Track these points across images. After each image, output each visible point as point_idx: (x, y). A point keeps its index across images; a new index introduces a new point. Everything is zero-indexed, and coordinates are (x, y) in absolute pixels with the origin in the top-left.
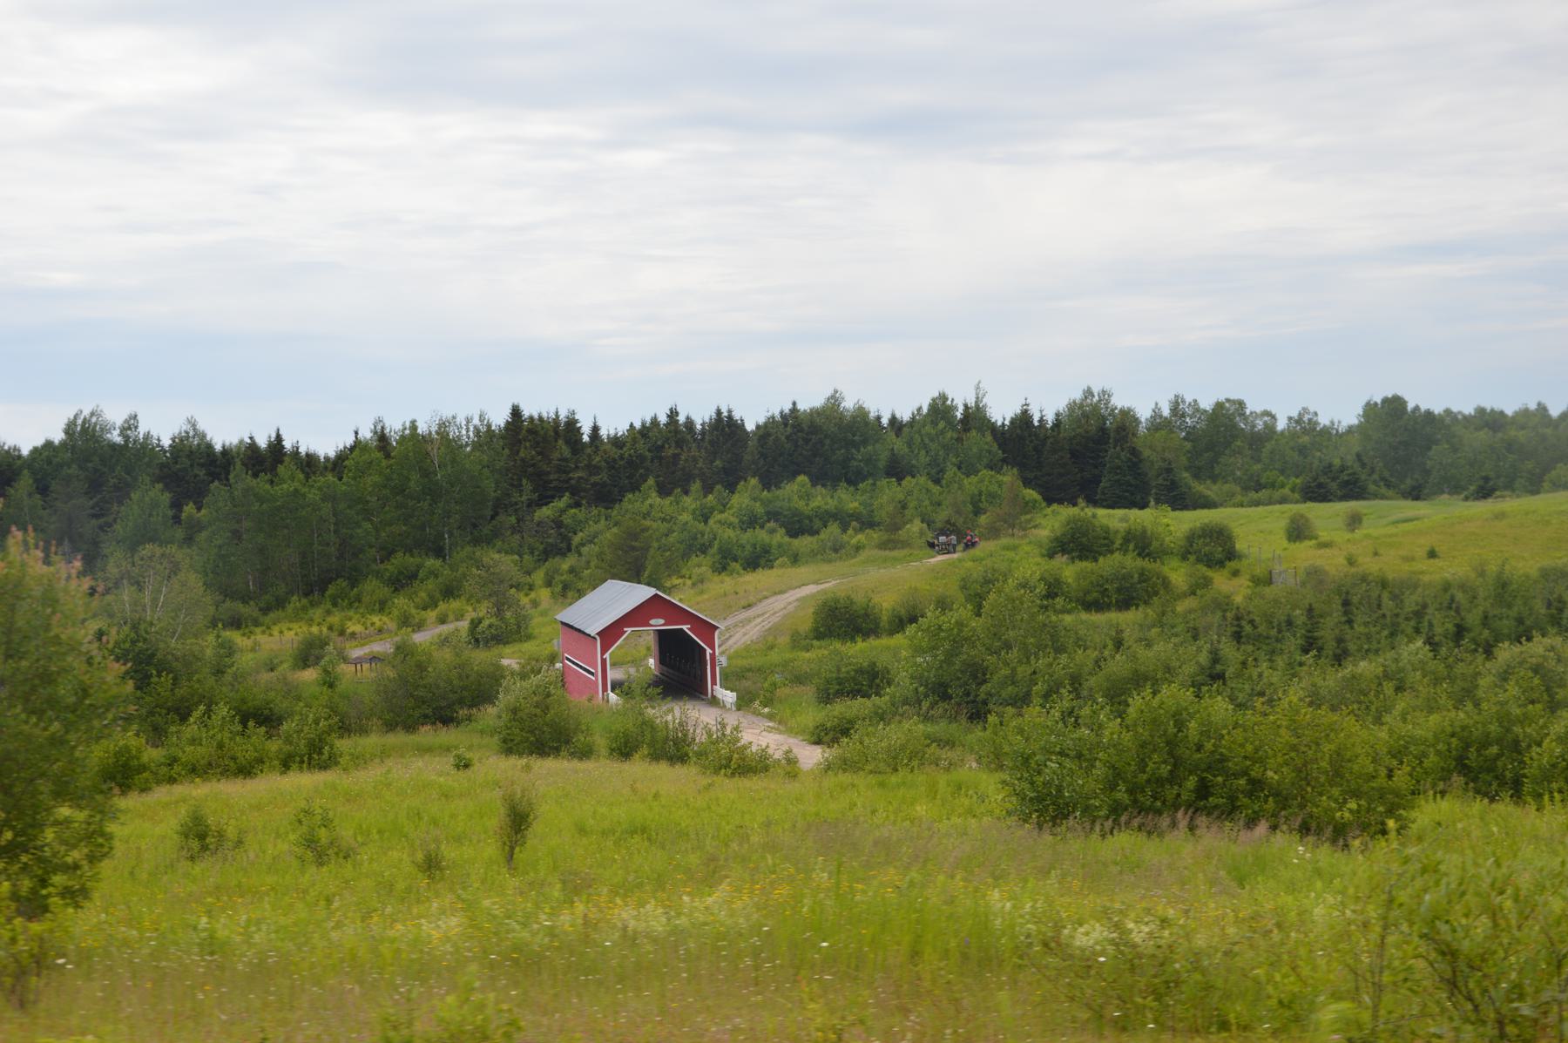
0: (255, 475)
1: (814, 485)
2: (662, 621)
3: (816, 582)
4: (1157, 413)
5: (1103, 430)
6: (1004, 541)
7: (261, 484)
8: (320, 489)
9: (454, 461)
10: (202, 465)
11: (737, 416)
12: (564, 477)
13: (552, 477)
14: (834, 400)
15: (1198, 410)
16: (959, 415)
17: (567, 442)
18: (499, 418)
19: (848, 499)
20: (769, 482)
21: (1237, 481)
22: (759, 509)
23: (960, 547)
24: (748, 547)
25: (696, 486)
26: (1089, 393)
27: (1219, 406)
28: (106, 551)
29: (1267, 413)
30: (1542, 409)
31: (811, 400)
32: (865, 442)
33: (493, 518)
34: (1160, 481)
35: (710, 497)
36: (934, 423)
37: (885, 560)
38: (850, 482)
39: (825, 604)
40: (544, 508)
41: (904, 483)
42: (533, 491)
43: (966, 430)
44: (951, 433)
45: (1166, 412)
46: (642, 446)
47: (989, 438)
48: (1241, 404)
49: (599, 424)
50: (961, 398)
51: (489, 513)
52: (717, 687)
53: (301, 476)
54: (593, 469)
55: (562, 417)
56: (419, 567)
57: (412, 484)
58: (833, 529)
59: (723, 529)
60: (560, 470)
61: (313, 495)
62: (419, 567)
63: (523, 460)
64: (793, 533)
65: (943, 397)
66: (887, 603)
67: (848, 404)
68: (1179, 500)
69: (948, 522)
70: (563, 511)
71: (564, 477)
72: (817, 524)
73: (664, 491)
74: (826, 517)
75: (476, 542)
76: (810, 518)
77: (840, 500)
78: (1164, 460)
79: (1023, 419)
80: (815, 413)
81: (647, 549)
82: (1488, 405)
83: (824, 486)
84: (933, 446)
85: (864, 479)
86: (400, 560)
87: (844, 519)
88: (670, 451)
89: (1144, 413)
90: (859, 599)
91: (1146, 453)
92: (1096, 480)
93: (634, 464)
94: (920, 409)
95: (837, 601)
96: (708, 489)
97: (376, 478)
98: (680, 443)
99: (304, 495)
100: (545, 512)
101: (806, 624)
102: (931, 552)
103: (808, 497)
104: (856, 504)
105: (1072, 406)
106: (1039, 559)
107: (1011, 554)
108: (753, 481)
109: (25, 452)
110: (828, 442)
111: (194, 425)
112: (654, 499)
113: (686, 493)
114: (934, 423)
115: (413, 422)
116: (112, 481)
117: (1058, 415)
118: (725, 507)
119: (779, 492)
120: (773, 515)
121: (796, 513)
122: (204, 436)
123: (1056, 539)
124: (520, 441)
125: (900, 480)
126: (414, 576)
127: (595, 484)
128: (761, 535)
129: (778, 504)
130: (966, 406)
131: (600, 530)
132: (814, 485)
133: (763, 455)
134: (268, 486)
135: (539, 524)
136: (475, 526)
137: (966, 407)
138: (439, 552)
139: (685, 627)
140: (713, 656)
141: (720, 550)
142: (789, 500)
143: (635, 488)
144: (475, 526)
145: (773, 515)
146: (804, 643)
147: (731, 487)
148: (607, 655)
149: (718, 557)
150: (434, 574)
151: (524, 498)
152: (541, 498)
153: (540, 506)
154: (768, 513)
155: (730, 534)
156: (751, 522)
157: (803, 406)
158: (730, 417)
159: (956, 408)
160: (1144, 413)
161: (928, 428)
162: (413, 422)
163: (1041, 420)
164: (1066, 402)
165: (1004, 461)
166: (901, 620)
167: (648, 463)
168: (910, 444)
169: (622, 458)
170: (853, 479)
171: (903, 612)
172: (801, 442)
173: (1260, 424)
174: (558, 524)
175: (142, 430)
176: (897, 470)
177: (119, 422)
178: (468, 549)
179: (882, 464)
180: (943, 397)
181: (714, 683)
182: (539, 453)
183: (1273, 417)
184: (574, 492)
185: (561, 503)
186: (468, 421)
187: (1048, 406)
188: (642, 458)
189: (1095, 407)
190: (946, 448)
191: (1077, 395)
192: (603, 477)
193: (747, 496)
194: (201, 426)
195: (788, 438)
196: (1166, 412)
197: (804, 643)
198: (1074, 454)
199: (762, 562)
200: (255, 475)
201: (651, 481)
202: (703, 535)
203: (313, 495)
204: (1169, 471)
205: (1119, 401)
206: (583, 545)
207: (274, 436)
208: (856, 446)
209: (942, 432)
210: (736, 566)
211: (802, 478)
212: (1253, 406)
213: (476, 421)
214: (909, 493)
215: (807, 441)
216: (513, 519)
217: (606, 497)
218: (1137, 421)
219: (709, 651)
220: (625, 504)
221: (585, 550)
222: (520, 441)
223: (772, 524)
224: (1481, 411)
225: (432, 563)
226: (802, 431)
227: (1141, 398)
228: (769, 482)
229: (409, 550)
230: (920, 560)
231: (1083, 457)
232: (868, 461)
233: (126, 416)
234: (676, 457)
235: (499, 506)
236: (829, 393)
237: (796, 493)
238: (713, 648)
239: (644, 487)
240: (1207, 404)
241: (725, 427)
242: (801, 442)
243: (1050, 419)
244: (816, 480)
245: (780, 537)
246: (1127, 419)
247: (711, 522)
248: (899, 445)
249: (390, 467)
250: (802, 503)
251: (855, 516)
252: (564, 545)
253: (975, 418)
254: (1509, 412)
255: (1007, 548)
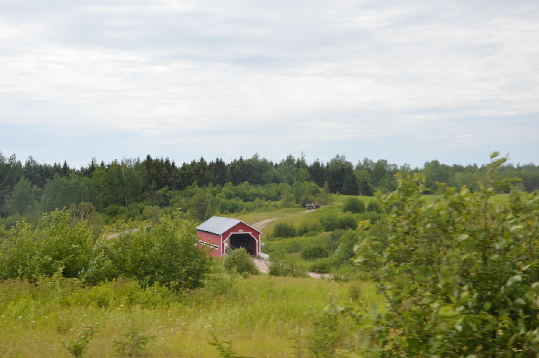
0: (62, 177)
1: (250, 184)
2: (242, 231)
3: (270, 218)
4: (359, 164)
5: (343, 169)
6: (328, 206)
7: (64, 179)
8: (84, 182)
9: (130, 174)
10: (39, 173)
11: (223, 160)
12: (166, 180)
13: (162, 180)
14: (256, 156)
15: (372, 163)
16: (296, 162)
17: (167, 168)
18: (143, 159)
19: (261, 190)
20: (235, 183)
21: (386, 187)
22: (232, 192)
23: (314, 207)
24: (231, 205)
25: (211, 184)
26: (338, 156)
27: (379, 162)
28: (6, 201)
29: (394, 165)
30: (475, 165)
31: (247, 157)
32: (266, 171)
33: (142, 193)
34: (363, 186)
35: (215, 188)
36: (289, 165)
37: (290, 211)
38: (262, 184)
39: (278, 226)
40: (160, 190)
41: (280, 184)
42: (156, 184)
43: (299, 168)
44: (293, 168)
45: (362, 164)
46: (192, 170)
47: (306, 170)
48: (386, 161)
49: (175, 162)
50: (296, 157)
51: (140, 191)
52: (260, 252)
53: (78, 177)
54: (176, 177)
55: (164, 160)
56: (118, 209)
57: (115, 181)
58: (258, 199)
59: (221, 198)
60: (165, 177)
61: (82, 184)
62: (118, 209)
63: (152, 174)
64: (245, 201)
65: (291, 156)
66: (297, 225)
67: (260, 158)
68: (369, 193)
69: (306, 199)
70: (166, 191)
71: (166, 180)
72: (252, 198)
73: (200, 185)
74: (255, 196)
75: (137, 201)
76: (249, 196)
77: (259, 190)
78: (364, 179)
79: (316, 164)
80: (251, 160)
81: (207, 205)
82: (458, 163)
83: (253, 185)
84: (288, 173)
85: (266, 183)
86: (111, 207)
87: (261, 197)
88: (201, 172)
89: (355, 164)
90: (289, 224)
91: (358, 177)
92: (341, 186)
93: (189, 176)
94: (283, 160)
95: (282, 224)
96: (215, 185)
97: (104, 179)
98: (205, 169)
99: (79, 184)
100: (160, 192)
101: (271, 232)
102: (304, 209)
103: (248, 188)
104: (264, 192)
105: (333, 161)
106: (341, 212)
107: (331, 210)
108: (230, 183)
109: (179, 165)
110: (254, 170)
111: (31, 159)
112: (197, 188)
113: (207, 186)
114: (289, 165)
115: (116, 160)
116: (7, 177)
117: (328, 163)
118: (220, 191)
119: (239, 187)
120: (237, 195)
121: (244, 194)
122: (35, 163)
123: (347, 206)
124: (150, 167)
125: (278, 184)
126: (117, 212)
127: (177, 183)
128: (234, 201)
129: (239, 191)
130: (298, 160)
131: (180, 199)
132: (250, 184)
133: (232, 174)
134: (67, 181)
135: (158, 196)
136: (136, 196)
137: (298, 160)
138: (124, 204)
139: (250, 233)
140: (258, 243)
141: (221, 206)
142: (242, 190)
143: (190, 184)
144: (136, 196)
145: (237, 195)
146: (271, 238)
147: (222, 185)
148: (224, 242)
149: (220, 208)
150: (124, 212)
151: (152, 187)
152: (158, 187)
153: (158, 189)
154: (235, 194)
155: (224, 200)
156: (229, 197)
157: (244, 158)
158: (221, 161)
159: (295, 160)
160: (355, 164)
161: (287, 167)
162: (116, 160)
163: (322, 165)
164: (379, 159)
165: (311, 178)
166: (302, 231)
167: (194, 176)
168: (280, 172)
169: (185, 174)
170: (263, 183)
171: (303, 229)
172: (245, 170)
173: (392, 168)
174: (165, 196)
175: (17, 160)
176: (276, 180)
177: (9, 157)
178: (135, 204)
179: (271, 179)
180: (116, 161)
181: (259, 251)
182: (157, 172)
183: (397, 166)
184: (170, 185)
185: (165, 189)
186: (134, 160)
187: (325, 160)
188: (192, 174)
189: (340, 161)
190: (293, 173)
191: (334, 157)
192: (180, 180)
193: (228, 187)
194: (34, 159)
195: (240, 169)
196: (362, 164)
197: (271, 238)
198: (334, 176)
199: (235, 210)
200: (62, 177)
201: (196, 182)
202: (215, 200)
203: (82, 184)
204: (366, 183)
205: (347, 159)
206: (174, 203)
207: (90, 163)
208: (263, 172)
209: (291, 168)
210: (226, 211)
211: (246, 182)
212: (390, 162)
213: (137, 160)
214: (282, 188)
215: (247, 170)
216: (149, 194)
217: (180, 187)
218: (352, 166)
219: (257, 241)
220: (187, 190)
221: (175, 205)
222: (150, 167)
223: (237, 198)
224: (455, 166)
225: (122, 208)
226: (245, 166)
227: (355, 160)
228: (235, 183)
229: (114, 203)
230: (302, 211)
231: (337, 177)
232: (267, 177)
233: (11, 155)
234: (203, 174)
235: (143, 189)
236: (254, 154)
237: (245, 187)
238: (258, 240)
239: (193, 184)
240: (375, 161)
241: (219, 164)
242: (245, 170)
243: (325, 165)
244: (251, 183)
245: (241, 202)
246: (349, 166)
247: (217, 196)
248: (276, 172)
249: (108, 175)
250: (247, 191)
251: (264, 196)
252: (166, 203)
253: (301, 164)
254: (464, 166)
255: (330, 208)
